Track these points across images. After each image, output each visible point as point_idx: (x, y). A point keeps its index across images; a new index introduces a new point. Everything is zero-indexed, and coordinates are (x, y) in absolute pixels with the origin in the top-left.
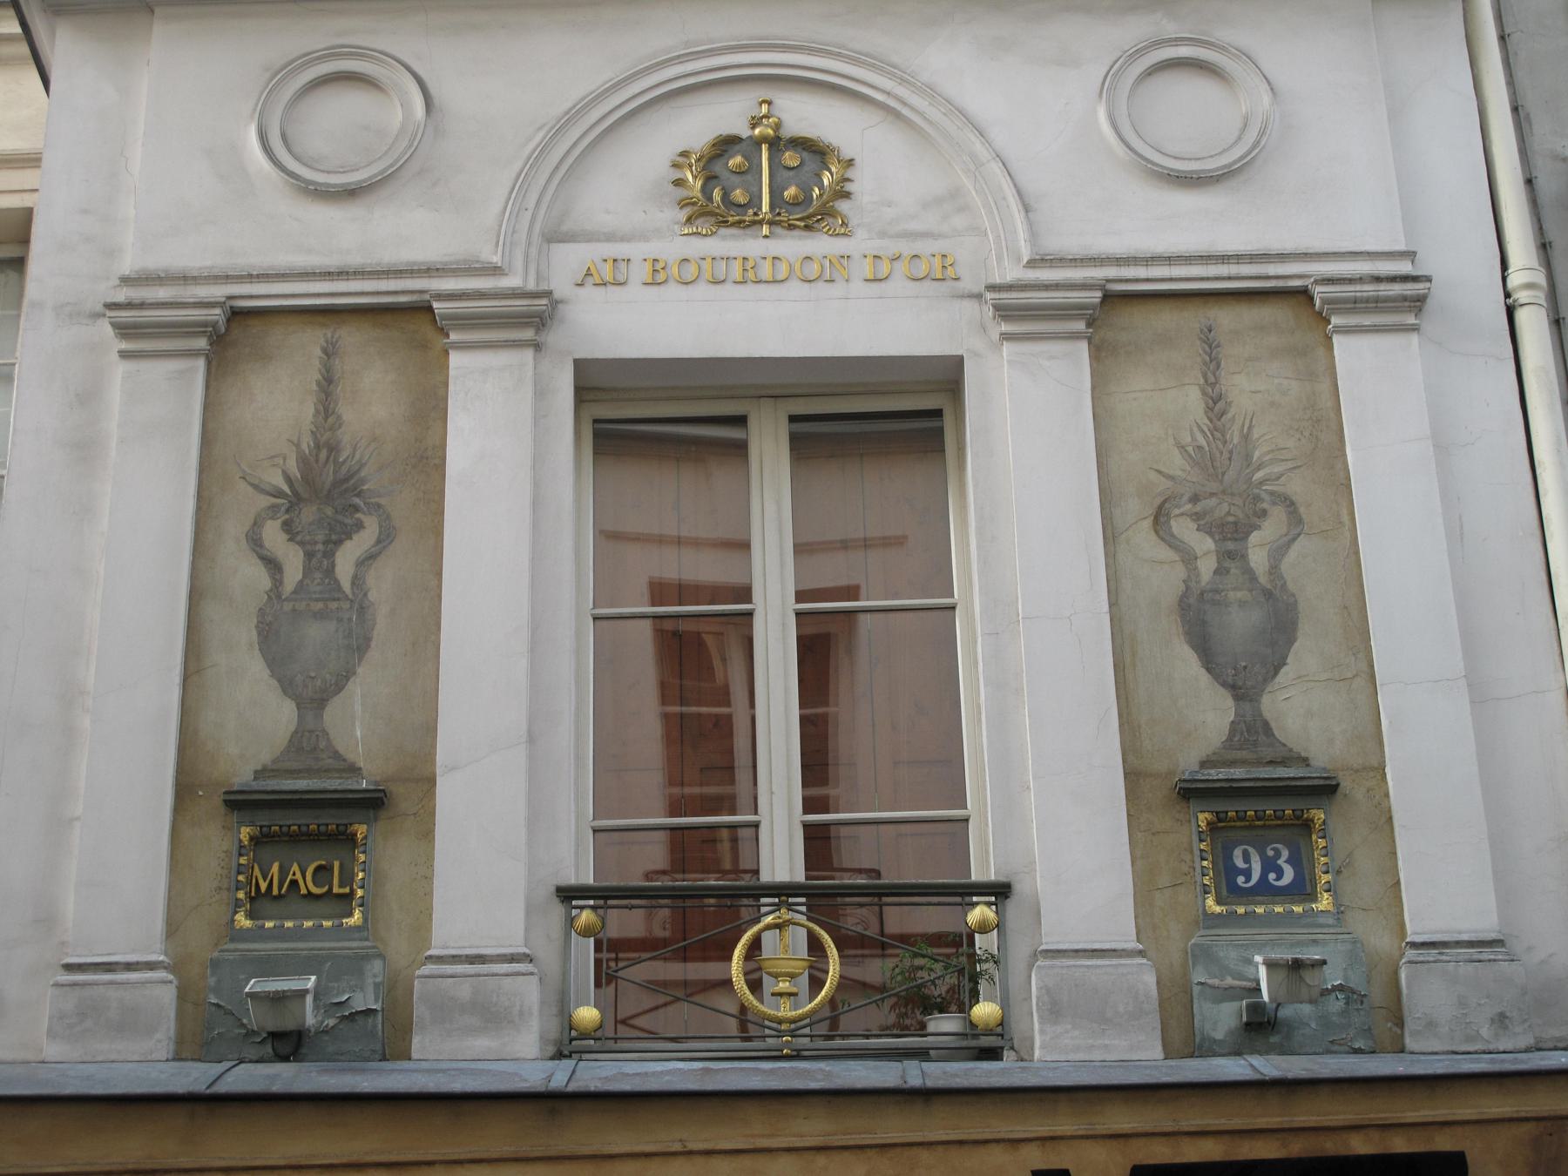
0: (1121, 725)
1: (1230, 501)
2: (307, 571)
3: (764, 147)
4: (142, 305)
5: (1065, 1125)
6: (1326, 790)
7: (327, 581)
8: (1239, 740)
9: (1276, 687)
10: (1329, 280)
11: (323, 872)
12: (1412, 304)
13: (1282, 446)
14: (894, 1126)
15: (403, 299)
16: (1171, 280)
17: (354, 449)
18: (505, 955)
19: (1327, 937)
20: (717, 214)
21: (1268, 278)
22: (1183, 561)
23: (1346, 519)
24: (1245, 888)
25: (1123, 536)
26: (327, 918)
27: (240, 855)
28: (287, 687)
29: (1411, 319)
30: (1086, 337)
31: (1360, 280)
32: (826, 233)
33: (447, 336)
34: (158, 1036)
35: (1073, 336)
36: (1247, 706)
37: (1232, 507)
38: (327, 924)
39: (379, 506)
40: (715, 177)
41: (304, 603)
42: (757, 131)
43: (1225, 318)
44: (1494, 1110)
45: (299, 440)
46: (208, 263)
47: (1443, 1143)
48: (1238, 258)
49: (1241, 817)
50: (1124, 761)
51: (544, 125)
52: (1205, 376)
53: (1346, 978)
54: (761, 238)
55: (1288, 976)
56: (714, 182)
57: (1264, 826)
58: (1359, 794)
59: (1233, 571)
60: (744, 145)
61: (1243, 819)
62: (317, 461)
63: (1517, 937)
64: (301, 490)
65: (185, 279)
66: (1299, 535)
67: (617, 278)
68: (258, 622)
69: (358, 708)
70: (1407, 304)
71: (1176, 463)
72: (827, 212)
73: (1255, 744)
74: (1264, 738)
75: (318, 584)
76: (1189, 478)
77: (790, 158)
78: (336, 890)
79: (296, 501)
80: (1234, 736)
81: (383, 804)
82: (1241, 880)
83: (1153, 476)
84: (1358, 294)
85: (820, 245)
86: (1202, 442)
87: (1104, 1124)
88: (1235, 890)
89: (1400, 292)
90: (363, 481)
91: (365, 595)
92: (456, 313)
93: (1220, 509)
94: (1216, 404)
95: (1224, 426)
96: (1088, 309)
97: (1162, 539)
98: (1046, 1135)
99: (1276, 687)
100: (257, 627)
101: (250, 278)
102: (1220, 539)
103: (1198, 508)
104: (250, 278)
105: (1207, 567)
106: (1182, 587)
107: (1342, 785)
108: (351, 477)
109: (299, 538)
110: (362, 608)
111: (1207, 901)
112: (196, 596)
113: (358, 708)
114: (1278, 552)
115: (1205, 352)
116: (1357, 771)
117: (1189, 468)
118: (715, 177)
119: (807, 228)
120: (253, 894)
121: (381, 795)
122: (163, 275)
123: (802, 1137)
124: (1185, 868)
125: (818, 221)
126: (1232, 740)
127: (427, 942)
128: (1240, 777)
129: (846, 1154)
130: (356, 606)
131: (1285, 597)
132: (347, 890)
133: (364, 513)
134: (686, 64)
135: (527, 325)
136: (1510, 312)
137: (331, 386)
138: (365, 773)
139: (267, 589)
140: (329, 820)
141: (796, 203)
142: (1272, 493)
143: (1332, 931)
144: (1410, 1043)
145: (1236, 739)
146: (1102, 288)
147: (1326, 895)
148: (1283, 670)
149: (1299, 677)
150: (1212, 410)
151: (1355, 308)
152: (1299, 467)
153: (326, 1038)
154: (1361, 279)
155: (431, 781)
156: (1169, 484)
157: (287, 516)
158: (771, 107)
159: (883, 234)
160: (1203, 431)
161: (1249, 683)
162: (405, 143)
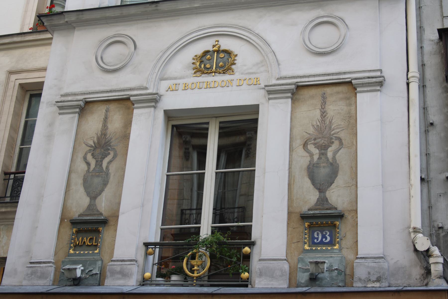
16: (314, 81)
20: (202, 71)
31: (364, 78)
35: (287, 98)
60: (211, 52)
71: (311, 130)
78: (94, 244)
83: (305, 134)
85: (226, 77)
88: (314, 244)
93: (321, 141)
94: (323, 114)
101: (90, 93)
105: (316, 157)
106: (309, 163)
109: (95, 157)
114: (335, 153)
119: (224, 73)
136: (408, 84)
140: (94, 227)
142: (336, 137)
156: (308, 136)
159: (242, 74)
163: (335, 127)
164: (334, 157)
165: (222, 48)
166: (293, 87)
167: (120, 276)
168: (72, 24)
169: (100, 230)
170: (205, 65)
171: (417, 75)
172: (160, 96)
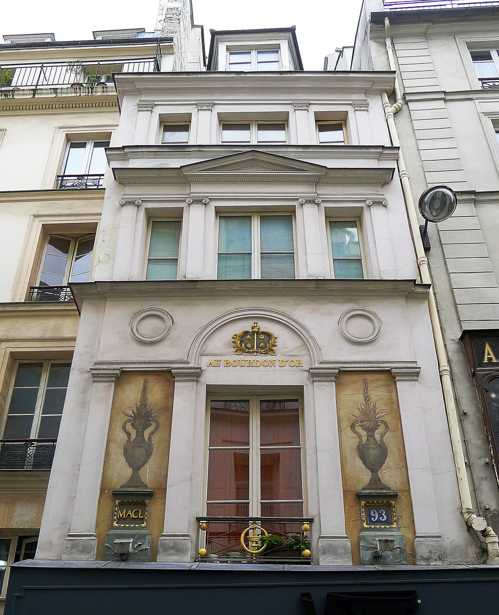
23: (400, 427)
28: (130, 465)
43: (369, 377)
48: (373, 362)
56: (242, 342)
58: (403, 497)
64: (136, 415)
65: (111, 363)
71: (357, 413)
77: (262, 337)
79: (135, 418)
85: (268, 358)
93: (368, 424)
94: (367, 398)
104: (127, 363)
105: (364, 439)
112: (108, 441)
114: (382, 435)
142: (381, 420)
146: (338, 369)
163: (379, 411)
164: (382, 440)
165: (261, 330)
167: (173, 552)
172: (202, 371)
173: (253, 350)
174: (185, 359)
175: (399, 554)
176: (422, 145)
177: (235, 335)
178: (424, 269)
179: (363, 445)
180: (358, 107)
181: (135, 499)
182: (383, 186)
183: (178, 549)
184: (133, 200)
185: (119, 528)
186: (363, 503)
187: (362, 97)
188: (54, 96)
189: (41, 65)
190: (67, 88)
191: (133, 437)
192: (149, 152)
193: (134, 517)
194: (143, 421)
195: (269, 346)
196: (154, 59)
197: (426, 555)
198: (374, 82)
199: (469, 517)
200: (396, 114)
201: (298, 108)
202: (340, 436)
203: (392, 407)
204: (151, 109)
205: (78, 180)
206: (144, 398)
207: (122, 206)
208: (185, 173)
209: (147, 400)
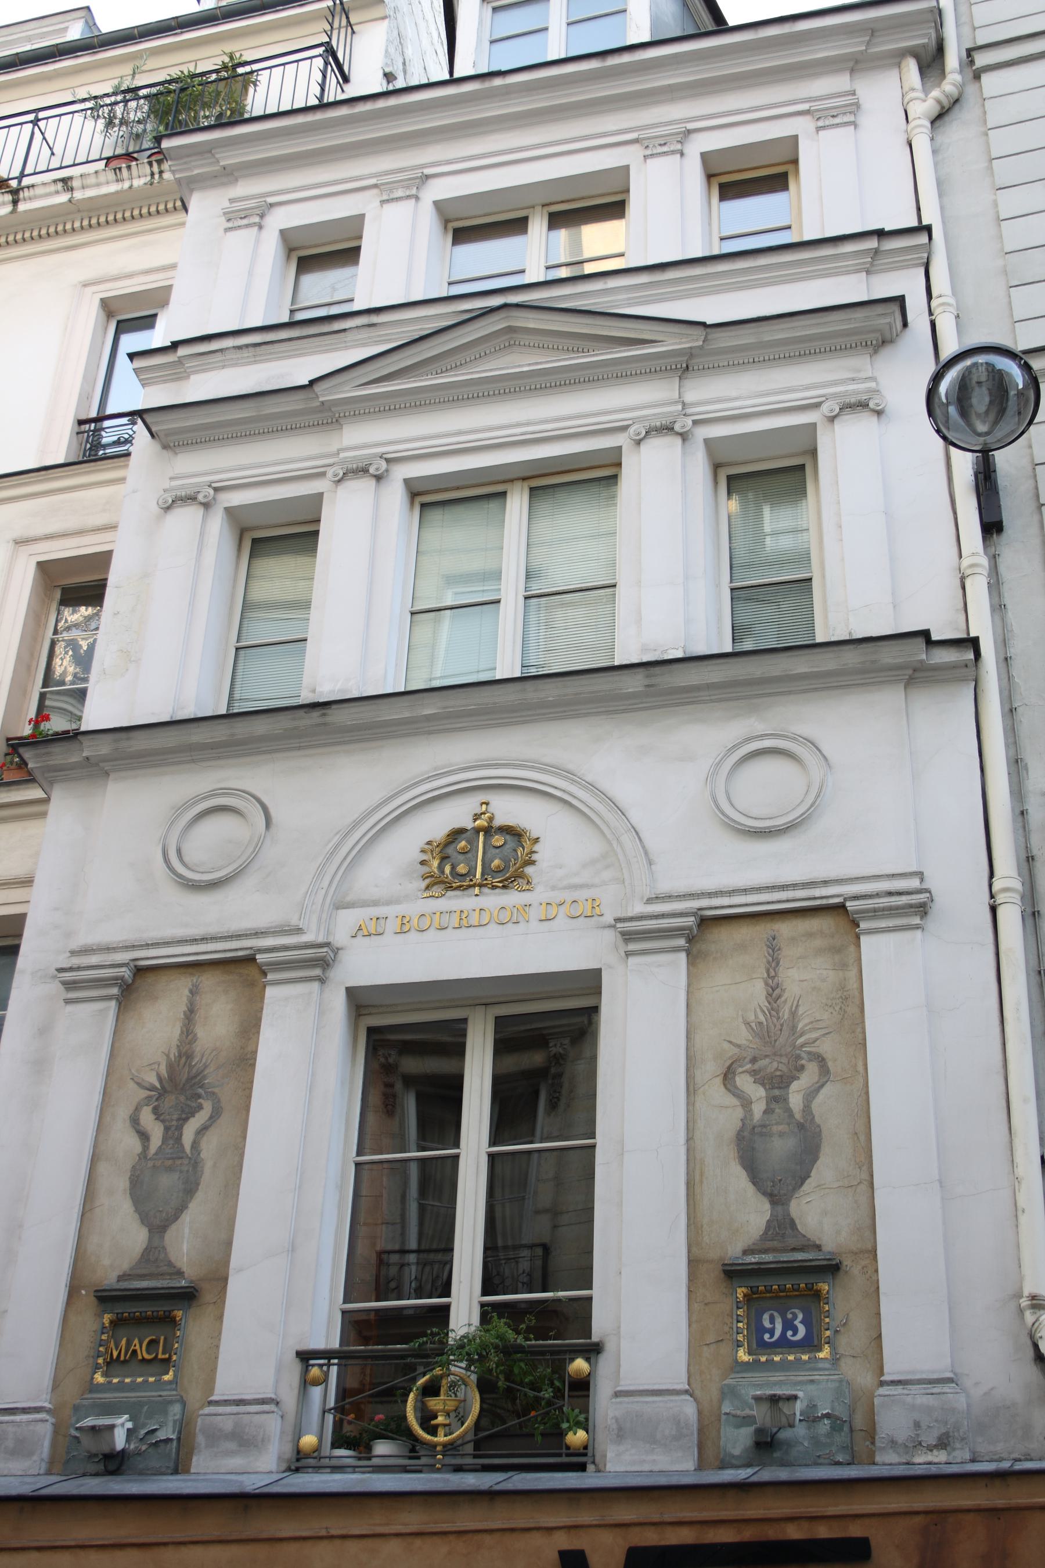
0: (689, 1225)
1: (779, 1060)
2: (165, 1140)
3: (481, 834)
4: (79, 968)
5: (585, 1517)
6: (832, 1269)
7: (176, 1146)
8: (772, 1234)
9: (802, 1193)
10: (855, 897)
11: (154, 1343)
12: (917, 910)
13: (819, 1019)
14: (467, 1519)
15: (240, 953)
16: (747, 905)
17: (202, 1056)
18: (258, 1399)
19: (822, 1377)
20: (446, 882)
21: (815, 898)
22: (742, 1106)
23: (861, 1068)
24: (771, 1342)
25: (702, 1089)
26: (152, 1376)
27: (103, 1333)
28: (144, 1218)
29: (916, 920)
30: (684, 950)
31: (878, 895)
32: (517, 890)
33: (858, 926)
34: (35, 1458)
35: (676, 950)
36: (779, 1208)
37: (780, 1065)
38: (152, 1379)
39: (214, 1093)
40: (448, 857)
41: (160, 1162)
42: (478, 822)
43: (785, 928)
44: (893, 1506)
45: (169, 1052)
46: (124, 938)
47: (855, 1531)
48: (794, 886)
49: (795, 1288)
50: (689, 1252)
51: (340, 831)
52: (768, 972)
53: (833, 1409)
54: (474, 897)
55: (771, 1407)
56: (446, 861)
57: (787, 1296)
58: (856, 1271)
59: (777, 1110)
60: (468, 833)
61: (771, 1291)
62: (178, 1065)
63: (967, 1375)
64: (166, 1085)
65: (109, 949)
66: (827, 1082)
67: (378, 930)
68: (131, 1175)
69: (187, 1231)
70: (913, 910)
71: (743, 1036)
72: (519, 875)
73: (783, 1236)
74: (790, 1231)
75: (170, 1148)
76: (751, 1046)
77: (498, 840)
78: (160, 1356)
79: (162, 1092)
80: (769, 1230)
81: (195, 1296)
82: (767, 1336)
83: (726, 1045)
84: (876, 906)
85: (512, 898)
86: (762, 1018)
87: (612, 1516)
89: (907, 902)
90: (205, 1077)
91: (199, 1154)
92: (630, 930)
93: (770, 1065)
94: (774, 992)
95: (778, 1006)
96: (685, 930)
97: (729, 1090)
98: (571, 1524)
99: (802, 1193)
100: (130, 1178)
101: (147, 946)
102: (769, 1088)
103: (756, 1067)
104: (147, 946)
105: (758, 1109)
106: (740, 1124)
107: (845, 1263)
108: (198, 1075)
109: (162, 1118)
110: (196, 1163)
111: (739, 1352)
112: (95, 1159)
113: (187, 1231)
114: (810, 1095)
115: (769, 954)
116: (856, 1253)
117: (751, 1038)
118: (448, 857)
119: (504, 887)
120: (108, 1360)
121: (192, 1290)
122: (95, 948)
123: (406, 1525)
124: (726, 1329)
125: (512, 882)
126: (767, 1234)
127: (211, 1390)
128: (769, 1260)
129: (435, 1538)
130: (192, 1162)
131: (813, 1128)
132: (167, 1356)
133: (203, 1099)
134: (433, 782)
135: (315, 966)
136: (993, 910)
137: (193, 1015)
138: (186, 1275)
139: (139, 1152)
140: (159, 1308)
141: (499, 871)
142: (809, 1053)
143: (827, 1373)
144: (878, 1459)
145: (770, 1233)
146: (694, 914)
147: (826, 1346)
148: (807, 1181)
149: (819, 1186)
150: (771, 995)
151: (875, 916)
152: (831, 1032)
153: (139, 1459)
154: (877, 894)
155: (225, 1279)
156: (736, 1050)
157: (156, 1103)
158: (489, 806)
159: (554, 888)
160: (763, 1012)
161: (782, 1192)
162: (251, 849)
163: (806, 1025)
164: (807, 1108)
165: (498, 822)
166: (690, 921)
167: (231, 1445)
168: (101, 764)
169: (178, 1319)
170: (453, 868)
171: (1017, 884)
172: (336, 951)
173: (471, 880)
174: (294, 921)
175: (829, 1435)
176: (1011, 203)
177: (429, 843)
178: (978, 589)
179: (754, 1128)
180: (826, 117)
181: (148, 1309)
182: (876, 352)
183: (245, 1437)
184: (190, 492)
185: (108, 1387)
186: (740, 1292)
187: (840, 82)
188: (64, 198)
189: (31, 117)
190: (96, 172)
191: (156, 1142)
192: (239, 348)
193: (147, 1356)
194: (182, 1098)
195: (515, 864)
196: (323, 48)
197: (902, 1436)
198: (873, 32)
199: (1034, 1320)
200: (940, 117)
201: (655, 152)
202: (690, 1104)
203: (845, 1012)
204: (257, 219)
205: (130, 426)
206: (187, 1036)
207: (168, 509)
208: (324, 395)
209: (196, 1040)
